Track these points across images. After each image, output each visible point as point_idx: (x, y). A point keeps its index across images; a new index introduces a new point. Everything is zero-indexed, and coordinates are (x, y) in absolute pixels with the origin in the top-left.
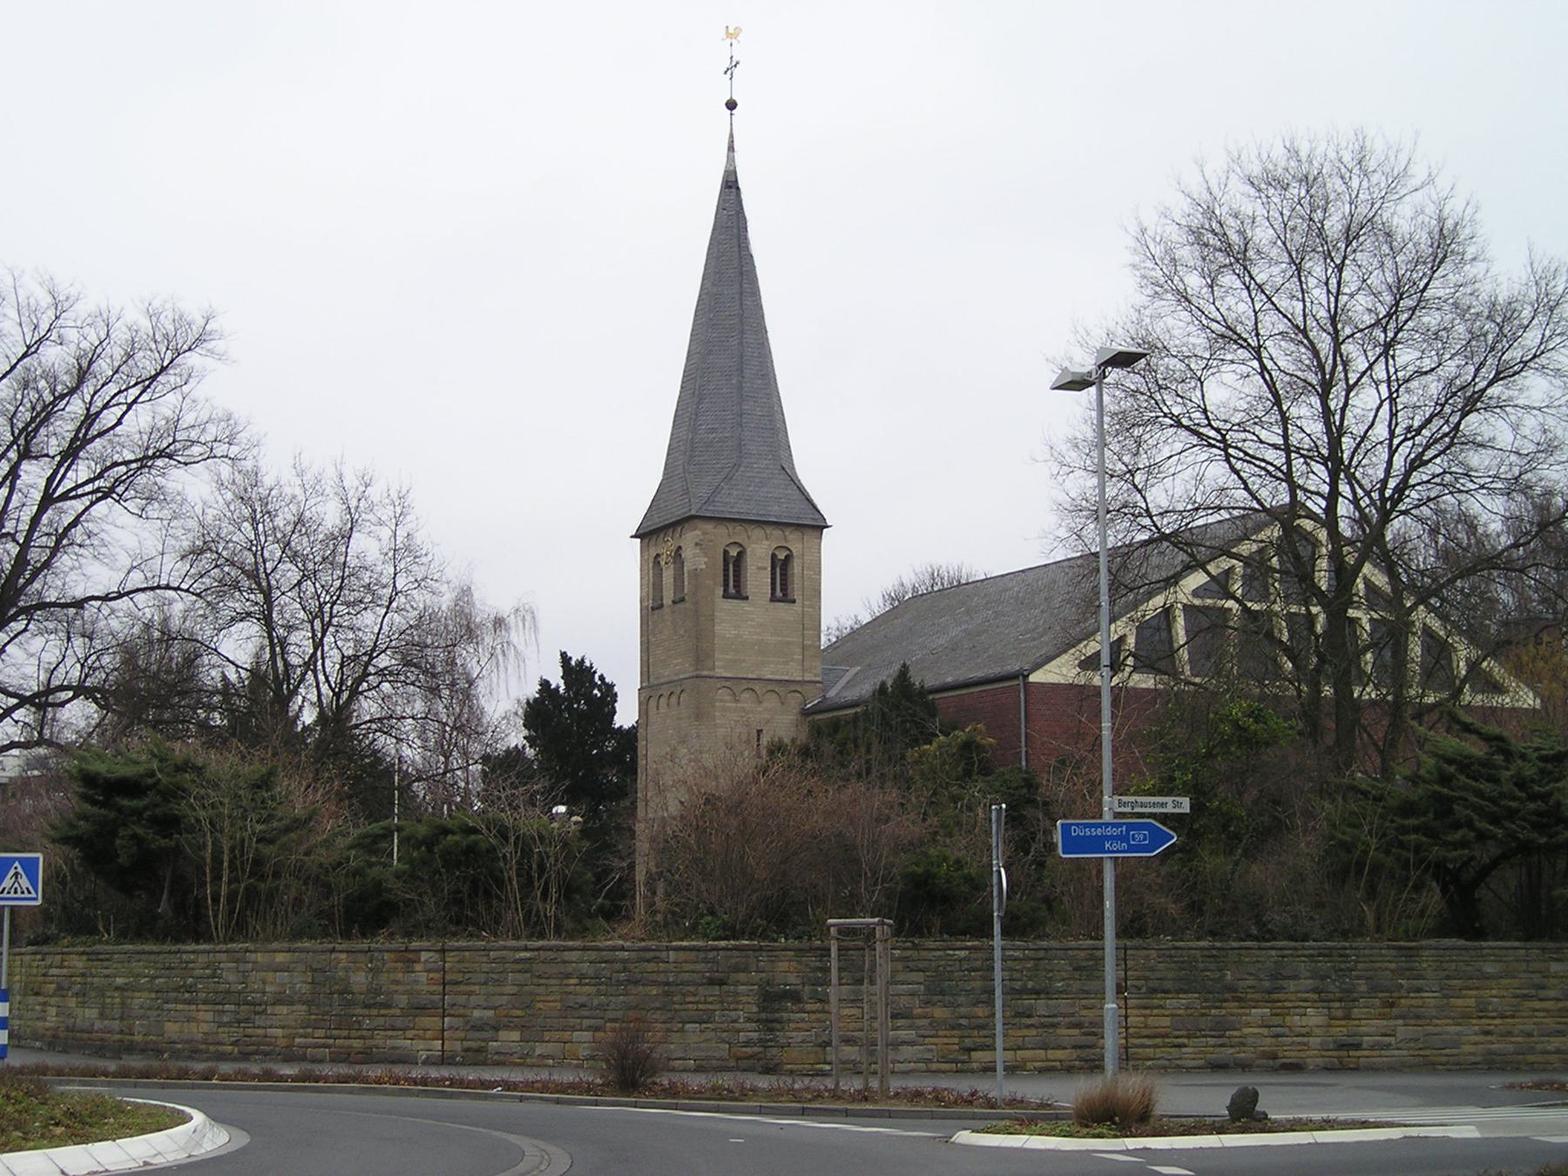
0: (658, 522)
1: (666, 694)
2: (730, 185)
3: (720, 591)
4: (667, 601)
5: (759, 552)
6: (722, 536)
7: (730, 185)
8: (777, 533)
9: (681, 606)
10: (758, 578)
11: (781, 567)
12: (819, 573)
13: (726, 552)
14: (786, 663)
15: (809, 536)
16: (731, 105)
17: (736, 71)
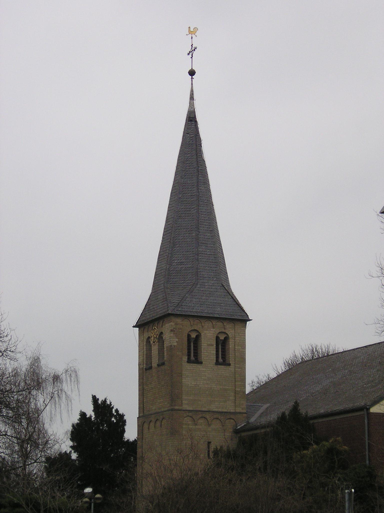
1: (153, 420)
2: (191, 119)
3: (185, 358)
4: (154, 365)
5: (209, 335)
7: (191, 119)
8: (220, 324)
9: (163, 367)
11: (222, 345)
12: (244, 348)
13: (189, 336)
16: (192, 73)
17: (195, 53)
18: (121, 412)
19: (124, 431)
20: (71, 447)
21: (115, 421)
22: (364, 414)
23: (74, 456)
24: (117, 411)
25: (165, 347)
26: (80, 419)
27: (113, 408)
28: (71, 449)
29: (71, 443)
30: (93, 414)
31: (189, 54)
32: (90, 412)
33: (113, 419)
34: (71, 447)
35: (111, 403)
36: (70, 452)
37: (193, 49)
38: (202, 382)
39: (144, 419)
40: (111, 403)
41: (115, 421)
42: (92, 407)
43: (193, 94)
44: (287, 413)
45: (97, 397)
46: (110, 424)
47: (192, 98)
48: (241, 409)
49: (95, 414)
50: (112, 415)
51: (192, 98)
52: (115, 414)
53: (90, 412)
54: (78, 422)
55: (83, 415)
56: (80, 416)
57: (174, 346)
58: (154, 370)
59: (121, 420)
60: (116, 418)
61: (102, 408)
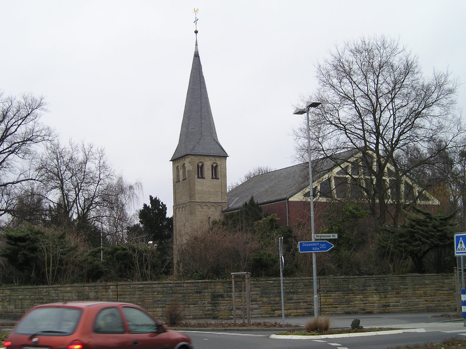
0: (178, 156)
2: (197, 56)
3: (197, 176)
4: (181, 180)
5: (208, 164)
6: (197, 160)
7: (197, 56)
9: (185, 181)
10: (208, 172)
11: (215, 169)
13: (198, 165)
14: (217, 197)
15: (223, 159)
16: (196, 32)
39: (176, 207)
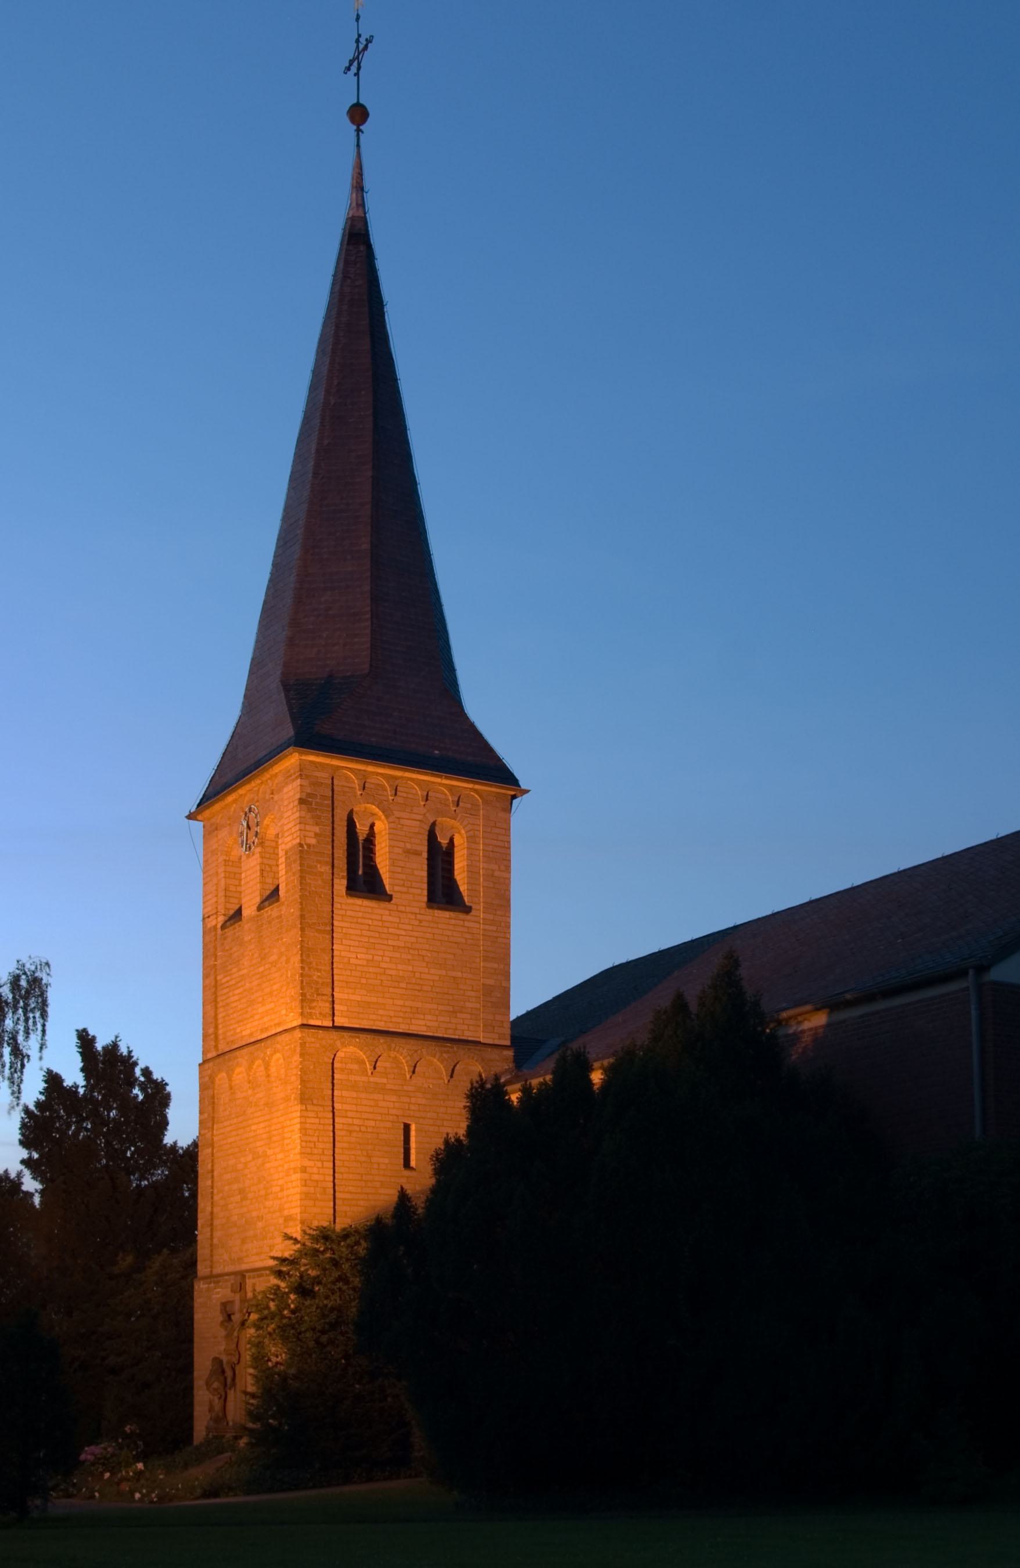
2: (357, 239)
7: (357, 239)
16: (359, 114)
18: (157, 1076)
19: (164, 1124)
20: (23, 1162)
21: (141, 1097)
22: (967, 989)
23: (30, 1184)
24: (147, 1072)
25: (281, 853)
26: (46, 1091)
27: (135, 1064)
28: (22, 1167)
29: (24, 1154)
30: (81, 1082)
31: (348, 69)
32: (73, 1076)
33: (136, 1091)
34: (23, 1162)
35: (130, 1052)
36: (19, 1175)
37: (361, 47)
38: (387, 953)
40: (130, 1052)
41: (141, 1097)
42: (78, 1062)
43: (361, 169)
44: (419, 1203)
45: (91, 1033)
46: (127, 1104)
47: (359, 187)
48: (497, 1036)
49: (87, 1078)
50: (131, 1082)
51: (359, 187)
52: (142, 1079)
53: (73, 1076)
54: (42, 1098)
55: (53, 1080)
56: (46, 1082)
57: (309, 846)
58: (246, 925)
59: (158, 1095)
60: (143, 1089)
61: (107, 1065)
